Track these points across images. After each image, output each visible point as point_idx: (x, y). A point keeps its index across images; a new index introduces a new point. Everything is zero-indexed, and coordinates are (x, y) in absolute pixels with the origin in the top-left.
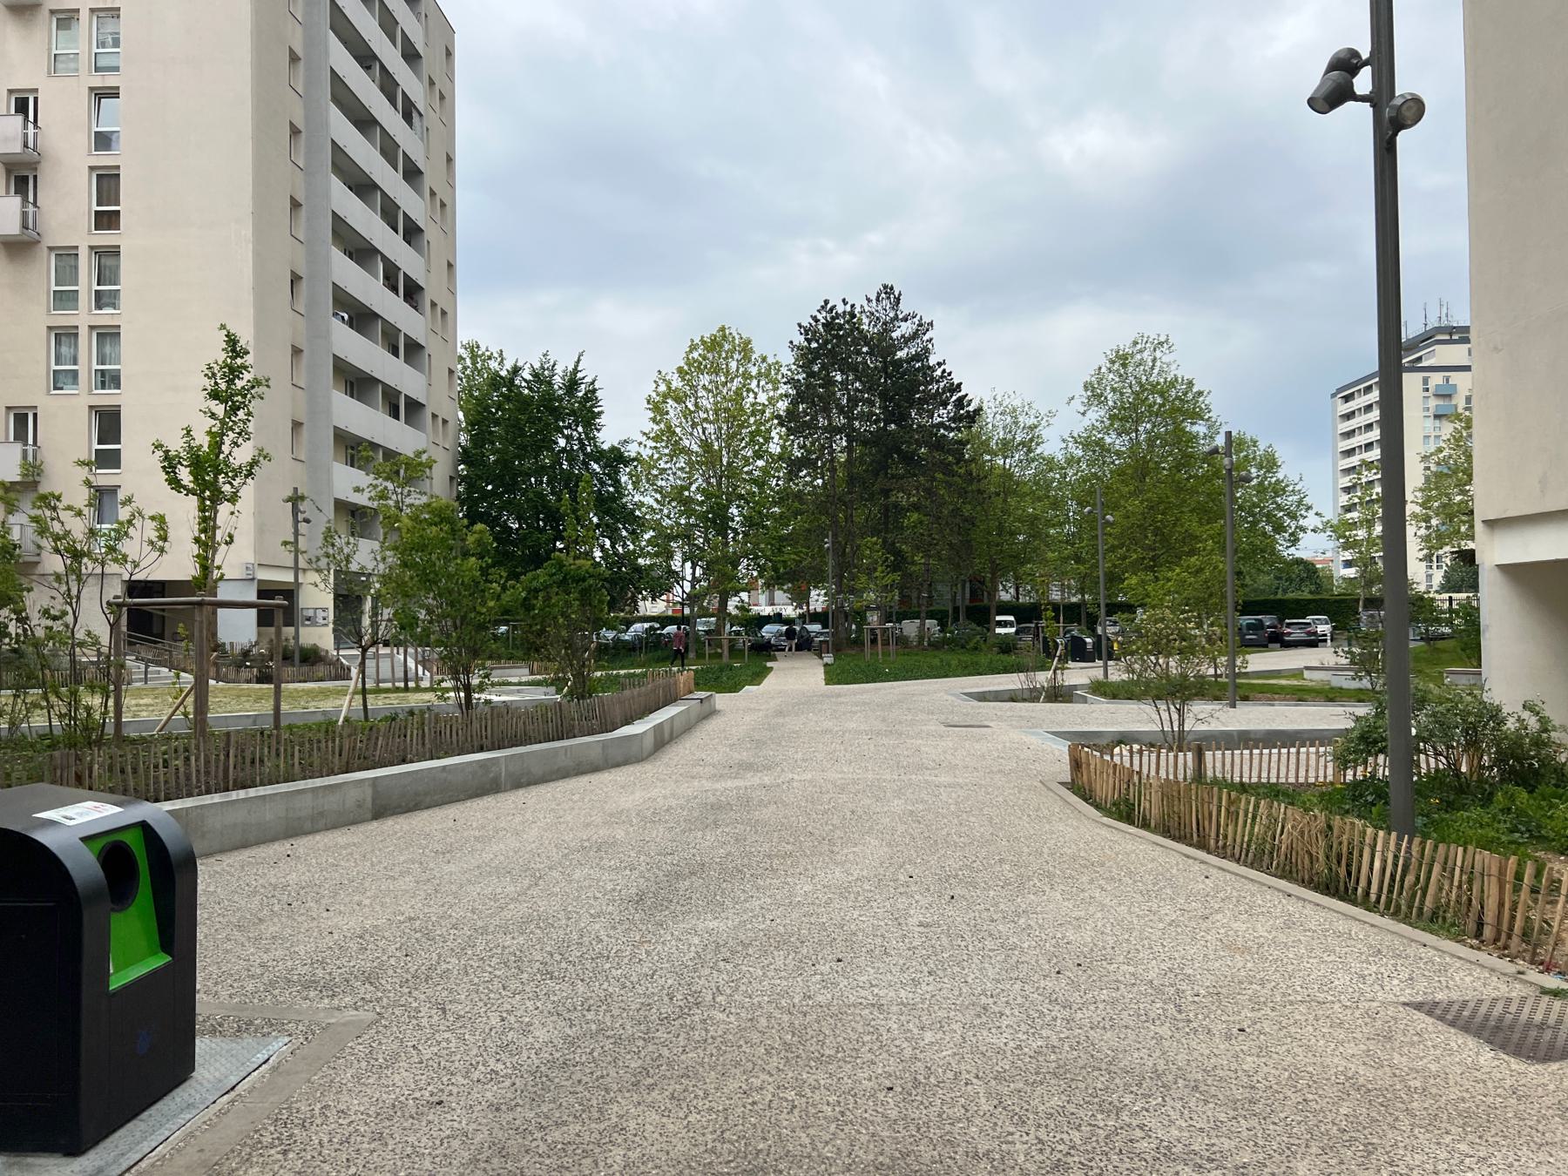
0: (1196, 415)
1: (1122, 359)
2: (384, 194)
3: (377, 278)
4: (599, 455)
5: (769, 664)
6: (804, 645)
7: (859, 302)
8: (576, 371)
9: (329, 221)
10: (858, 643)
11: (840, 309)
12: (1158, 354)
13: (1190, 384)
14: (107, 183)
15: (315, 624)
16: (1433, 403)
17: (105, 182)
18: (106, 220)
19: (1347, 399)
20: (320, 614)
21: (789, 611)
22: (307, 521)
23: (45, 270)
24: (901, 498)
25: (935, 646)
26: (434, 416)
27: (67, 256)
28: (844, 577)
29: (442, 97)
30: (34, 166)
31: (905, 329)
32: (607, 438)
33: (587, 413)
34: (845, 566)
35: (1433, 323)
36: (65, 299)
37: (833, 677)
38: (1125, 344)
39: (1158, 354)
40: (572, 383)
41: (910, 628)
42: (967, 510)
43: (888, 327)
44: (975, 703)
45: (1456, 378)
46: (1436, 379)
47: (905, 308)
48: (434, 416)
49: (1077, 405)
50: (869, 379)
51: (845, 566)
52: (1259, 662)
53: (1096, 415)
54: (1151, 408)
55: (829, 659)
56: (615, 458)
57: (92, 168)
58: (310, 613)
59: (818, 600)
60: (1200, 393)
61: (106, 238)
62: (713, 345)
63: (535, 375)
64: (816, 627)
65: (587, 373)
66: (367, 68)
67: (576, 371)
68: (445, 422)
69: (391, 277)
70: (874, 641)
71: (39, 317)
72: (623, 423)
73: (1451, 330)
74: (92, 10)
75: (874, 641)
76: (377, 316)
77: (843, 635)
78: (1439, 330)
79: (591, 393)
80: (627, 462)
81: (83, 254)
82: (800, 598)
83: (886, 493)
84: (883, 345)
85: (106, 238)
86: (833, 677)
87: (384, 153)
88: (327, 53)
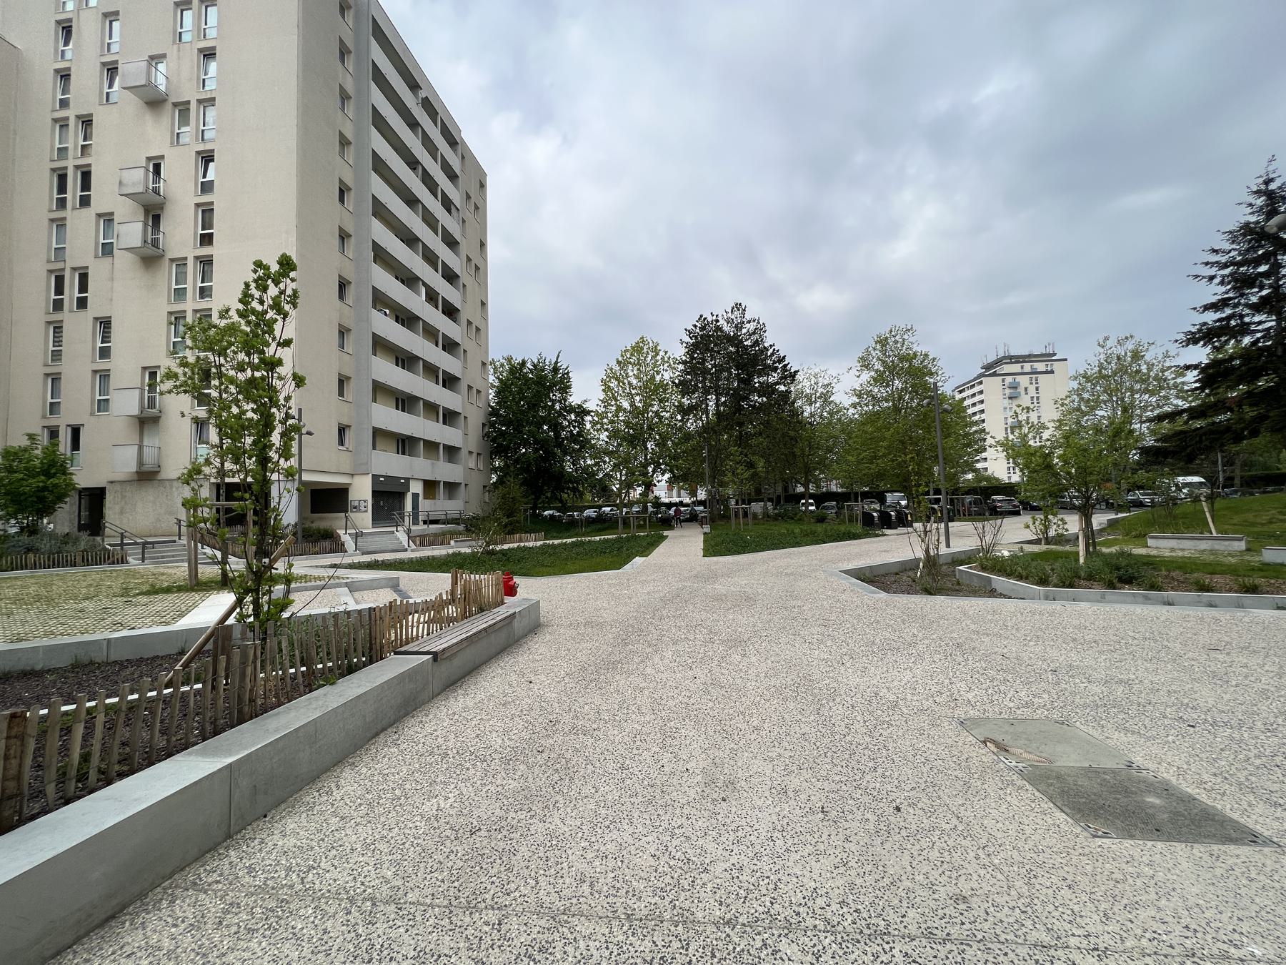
0: (931, 374)
1: (883, 342)
2: (424, 244)
3: (419, 295)
4: (571, 409)
5: (665, 533)
6: (693, 518)
7: (720, 312)
8: (556, 363)
9: (371, 244)
10: (726, 517)
11: (710, 319)
12: (906, 337)
13: (926, 355)
14: (207, 213)
15: (360, 511)
16: (1008, 391)
17: (207, 215)
18: (207, 240)
19: (961, 392)
20: (363, 504)
21: (687, 500)
22: (309, 433)
23: (166, 274)
24: (750, 429)
25: (775, 518)
26: (470, 387)
27: (181, 263)
28: (716, 477)
29: (477, 208)
30: (161, 206)
31: (752, 326)
32: (574, 399)
33: (564, 385)
34: (716, 473)
35: (1001, 354)
36: (180, 294)
37: (712, 549)
38: (884, 331)
39: (906, 337)
40: (556, 370)
41: (757, 507)
42: (792, 433)
43: (738, 327)
44: (1226, 807)
45: (1018, 378)
46: (1009, 379)
47: (748, 317)
48: (470, 387)
49: (854, 372)
50: (731, 361)
51: (716, 473)
52: (1162, 546)
53: (866, 376)
54: (904, 370)
55: (707, 529)
56: (582, 412)
57: (198, 205)
58: (356, 504)
59: (702, 494)
60: (934, 359)
61: (205, 251)
62: (637, 349)
63: (535, 366)
64: (701, 508)
65: (563, 364)
66: (414, 169)
67: (556, 363)
68: (478, 392)
69: (432, 297)
70: (736, 515)
71: (163, 306)
72: (586, 390)
73: (1011, 357)
74: (199, 101)
75: (736, 515)
76: (418, 318)
77: (716, 512)
78: (1004, 358)
79: (566, 375)
80: (588, 413)
81: (190, 262)
82: (693, 493)
83: (741, 424)
84: (735, 340)
85: (205, 251)
86: (712, 549)
87: (424, 220)
88: (369, 139)
